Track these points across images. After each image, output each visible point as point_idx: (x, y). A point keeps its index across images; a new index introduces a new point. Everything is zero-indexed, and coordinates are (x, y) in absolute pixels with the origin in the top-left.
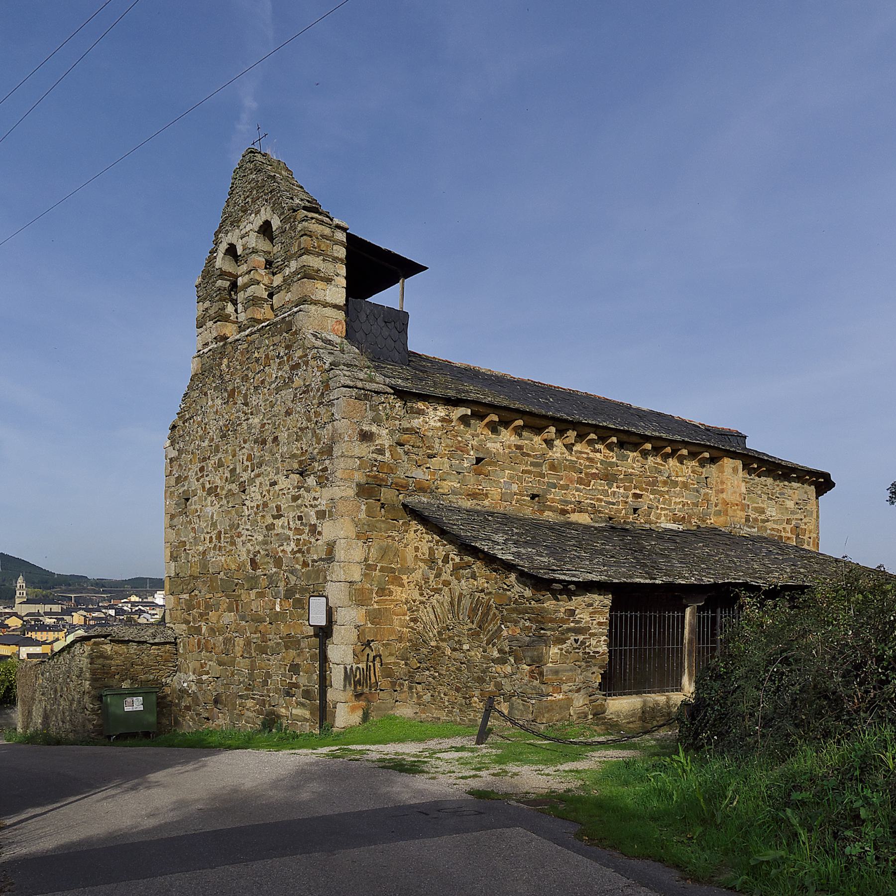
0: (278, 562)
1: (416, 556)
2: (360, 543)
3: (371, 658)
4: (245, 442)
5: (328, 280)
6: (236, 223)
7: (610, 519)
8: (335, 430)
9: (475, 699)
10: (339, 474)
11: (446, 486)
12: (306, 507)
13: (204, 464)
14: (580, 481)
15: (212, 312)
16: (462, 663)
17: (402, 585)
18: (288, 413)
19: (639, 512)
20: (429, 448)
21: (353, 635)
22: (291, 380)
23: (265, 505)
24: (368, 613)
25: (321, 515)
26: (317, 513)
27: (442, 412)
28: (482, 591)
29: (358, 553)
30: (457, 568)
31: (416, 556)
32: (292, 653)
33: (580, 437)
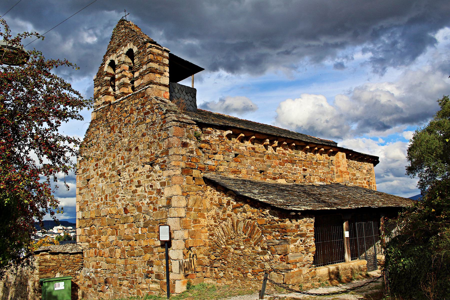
0: (139, 209)
1: (211, 203)
2: (184, 198)
3: (192, 256)
4: (120, 150)
5: (161, 74)
6: (114, 51)
7: (295, 181)
8: (169, 143)
9: (250, 274)
10: (173, 163)
12: (154, 180)
13: (98, 162)
14: (280, 164)
15: (102, 91)
16: (240, 256)
17: (205, 218)
18: (143, 135)
19: (306, 177)
20: (213, 150)
21: (182, 245)
22: (145, 119)
23: (132, 181)
24: (189, 233)
25: (163, 184)
27: (218, 132)
28: (250, 218)
29: (183, 203)
30: (234, 208)
31: (211, 203)
32: (148, 255)
33: (280, 145)
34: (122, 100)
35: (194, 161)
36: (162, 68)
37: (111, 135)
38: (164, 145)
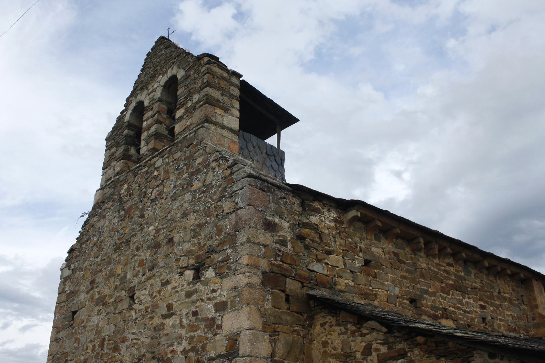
2: (267, 337)
4: (138, 249)
5: (226, 110)
8: (239, 218)
11: (343, 282)
12: (202, 300)
14: (443, 290)
15: (117, 154)
19: (487, 320)
22: (190, 184)
26: (215, 305)
31: (325, 352)
34: (150, 160)
35: (289, 261)
36: (226, 100)
37: (124, 224)
38: (227, 225)
